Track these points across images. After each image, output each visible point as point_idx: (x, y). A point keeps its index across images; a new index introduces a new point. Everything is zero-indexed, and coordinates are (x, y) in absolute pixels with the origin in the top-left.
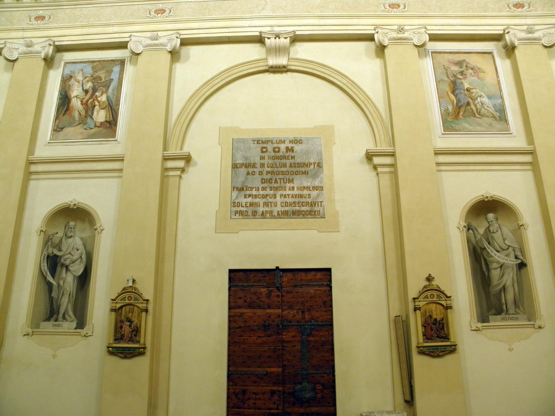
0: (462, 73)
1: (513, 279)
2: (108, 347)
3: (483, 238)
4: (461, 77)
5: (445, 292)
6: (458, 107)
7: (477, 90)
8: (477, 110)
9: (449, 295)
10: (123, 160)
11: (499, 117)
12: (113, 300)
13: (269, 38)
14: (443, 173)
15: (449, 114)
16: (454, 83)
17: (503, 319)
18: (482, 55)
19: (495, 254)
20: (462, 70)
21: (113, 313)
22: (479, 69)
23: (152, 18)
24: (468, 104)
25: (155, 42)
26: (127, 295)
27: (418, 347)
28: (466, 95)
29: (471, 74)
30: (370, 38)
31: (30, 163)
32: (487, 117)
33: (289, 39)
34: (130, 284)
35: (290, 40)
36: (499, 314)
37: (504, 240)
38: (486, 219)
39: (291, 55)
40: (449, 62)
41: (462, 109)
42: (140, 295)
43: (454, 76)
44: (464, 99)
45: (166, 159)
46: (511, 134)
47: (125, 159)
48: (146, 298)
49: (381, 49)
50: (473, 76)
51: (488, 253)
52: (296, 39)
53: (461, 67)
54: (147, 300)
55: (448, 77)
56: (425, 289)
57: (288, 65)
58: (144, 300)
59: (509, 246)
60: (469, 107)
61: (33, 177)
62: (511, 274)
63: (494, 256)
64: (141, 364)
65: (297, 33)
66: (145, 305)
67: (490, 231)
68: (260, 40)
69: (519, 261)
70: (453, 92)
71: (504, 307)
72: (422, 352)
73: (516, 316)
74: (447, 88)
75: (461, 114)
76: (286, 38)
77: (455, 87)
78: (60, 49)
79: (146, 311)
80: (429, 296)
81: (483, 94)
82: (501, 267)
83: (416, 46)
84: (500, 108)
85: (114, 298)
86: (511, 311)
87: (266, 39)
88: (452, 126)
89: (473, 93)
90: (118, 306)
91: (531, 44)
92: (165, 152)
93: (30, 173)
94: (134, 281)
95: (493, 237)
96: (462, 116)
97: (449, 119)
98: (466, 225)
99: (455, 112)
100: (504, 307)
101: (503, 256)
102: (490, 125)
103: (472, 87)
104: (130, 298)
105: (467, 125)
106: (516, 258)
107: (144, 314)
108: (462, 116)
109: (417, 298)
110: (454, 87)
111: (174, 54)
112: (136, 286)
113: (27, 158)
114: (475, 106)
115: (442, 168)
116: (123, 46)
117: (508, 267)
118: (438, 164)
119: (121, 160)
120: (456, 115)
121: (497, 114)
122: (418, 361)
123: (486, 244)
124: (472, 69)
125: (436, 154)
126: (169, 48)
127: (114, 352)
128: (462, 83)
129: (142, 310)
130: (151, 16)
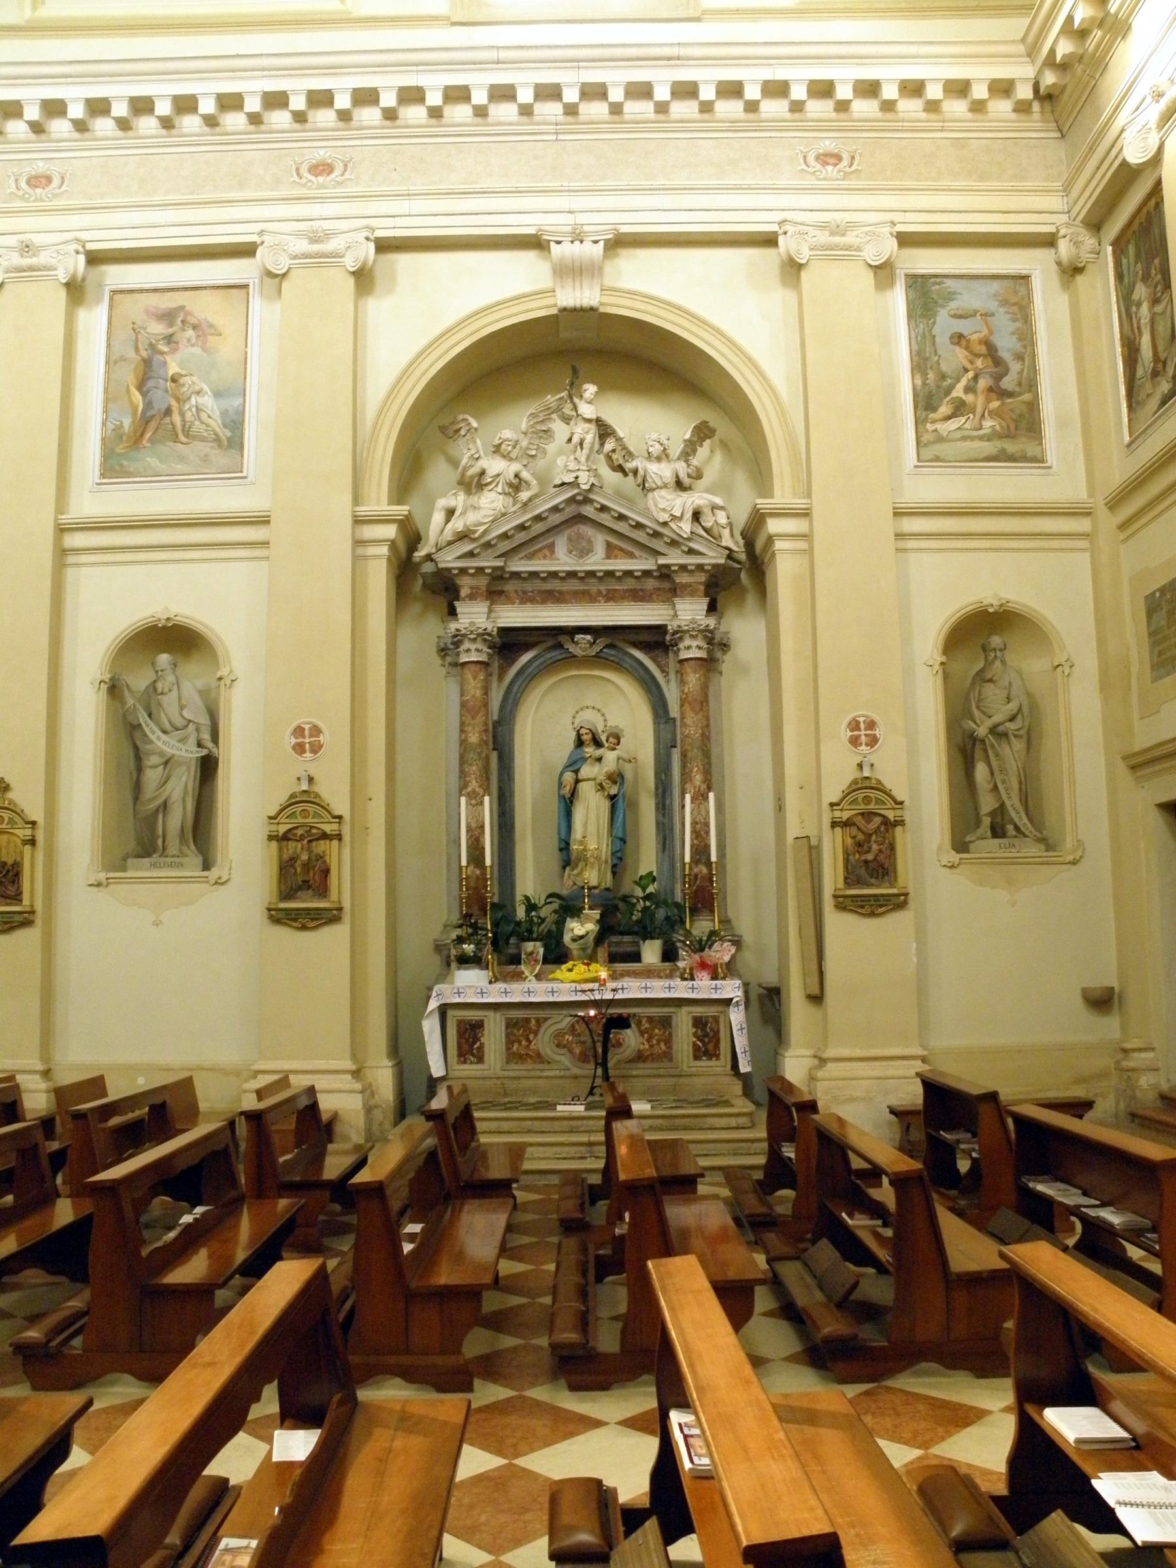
0: (169, 339)
1: (186, 787)
2: (269, 910)
3: (138, 706)
4: (166, 349)
5: (893, 793)
6: (144, 421)
7: (195, 379)
8: (184, 426)
9: (899, 799)
10: (268, 522)
11: (229, 439)
12: (270, 818)
13: (559, 243)
14: (912, 556)
15: (121, 438)
16: (147, 363)
17: (154, 866)
18: (222, 291)
19: (158, 738)
20: (170, 331)
21: (274, 844)
22: (211, 326)
23: (304, 185)
24: (168, 412)
25: (837, 239)
26: (298, 808)
27: (835, 897)
28: (167, 391)
29: (189, 340)
30: (769, 241)
31: (61, 530)
32: (204, 439)
33: (602, 243)
34: (305, 787)
35: (605, 245)
36: (149, 855)
37: (182, 708)
38: (153, 664)
40: (147, 312)
41: (153, 425)
42: (20, 814)
43: (152, 347)
44: (161, 400)
45: (358, 521)
46: (1050, 468)
47: (272, 519)
48: (337, 813)
49: (793, 269)
50: (193, 345)
51: (146, 735)
52: (619, 243)
53: (171, 325)
54: (340, 817)
55: (137, 349)
56: (854, 787)
59: (190, 721)
60: (167, 420)
61: (71, 559)
62: (184, 779)
63: (155, 741)
64: (895, 923)
65: (624, 229)
66: (335, 827)
67: (155, 690)
68: (535, 243)
69: (205, 752)
70: (140, 387)
71: (160, 842)
72: (843, 904)
73: (180, 860)
74: (127, 375)
75: (148, 435)
76: (596, 242)
77: (147, 372)
78: (95, 259)
80: (860, 799)
81: (206, 388)
82: (166, 763)
83: (871, 266)
84: (234, 418)
85: (273, 814)
86: (173, 849)
87: (552, 244)
88: (121, 466)
89: (184, 385)
90: (282, 829)
91: (320, 265)
92: (357, 509)
93: (64, 550)
94: (311, 780)
95: (159, 704)
96: (149, 440)
97: (119, 450)
98: (107, 677)
99: (135, 432)
100: (160, 842)
101: (173, 742)
102: (205, 459)
103: (183, 372)
104: (867, 800)
105: (153, 462)
106: (200, 745)
108: (149, 440)
109: (838, 804)
110: (145, 374)
111: (363, 278)
112: (316, 789)
113: (56, 519)
114: (182, 415)
115: (912, 544)
116: (246, 251)
117: (180, 764)
118: (899, 536)
119: (264, 521)
120: (136, 440)
121: (224, 434)
122: (837, 924)
123: (143, 717)
124: (195, 327)
126: (351, 263)
127: (278, 917)
128: (166, 363)
130: (303, 181)
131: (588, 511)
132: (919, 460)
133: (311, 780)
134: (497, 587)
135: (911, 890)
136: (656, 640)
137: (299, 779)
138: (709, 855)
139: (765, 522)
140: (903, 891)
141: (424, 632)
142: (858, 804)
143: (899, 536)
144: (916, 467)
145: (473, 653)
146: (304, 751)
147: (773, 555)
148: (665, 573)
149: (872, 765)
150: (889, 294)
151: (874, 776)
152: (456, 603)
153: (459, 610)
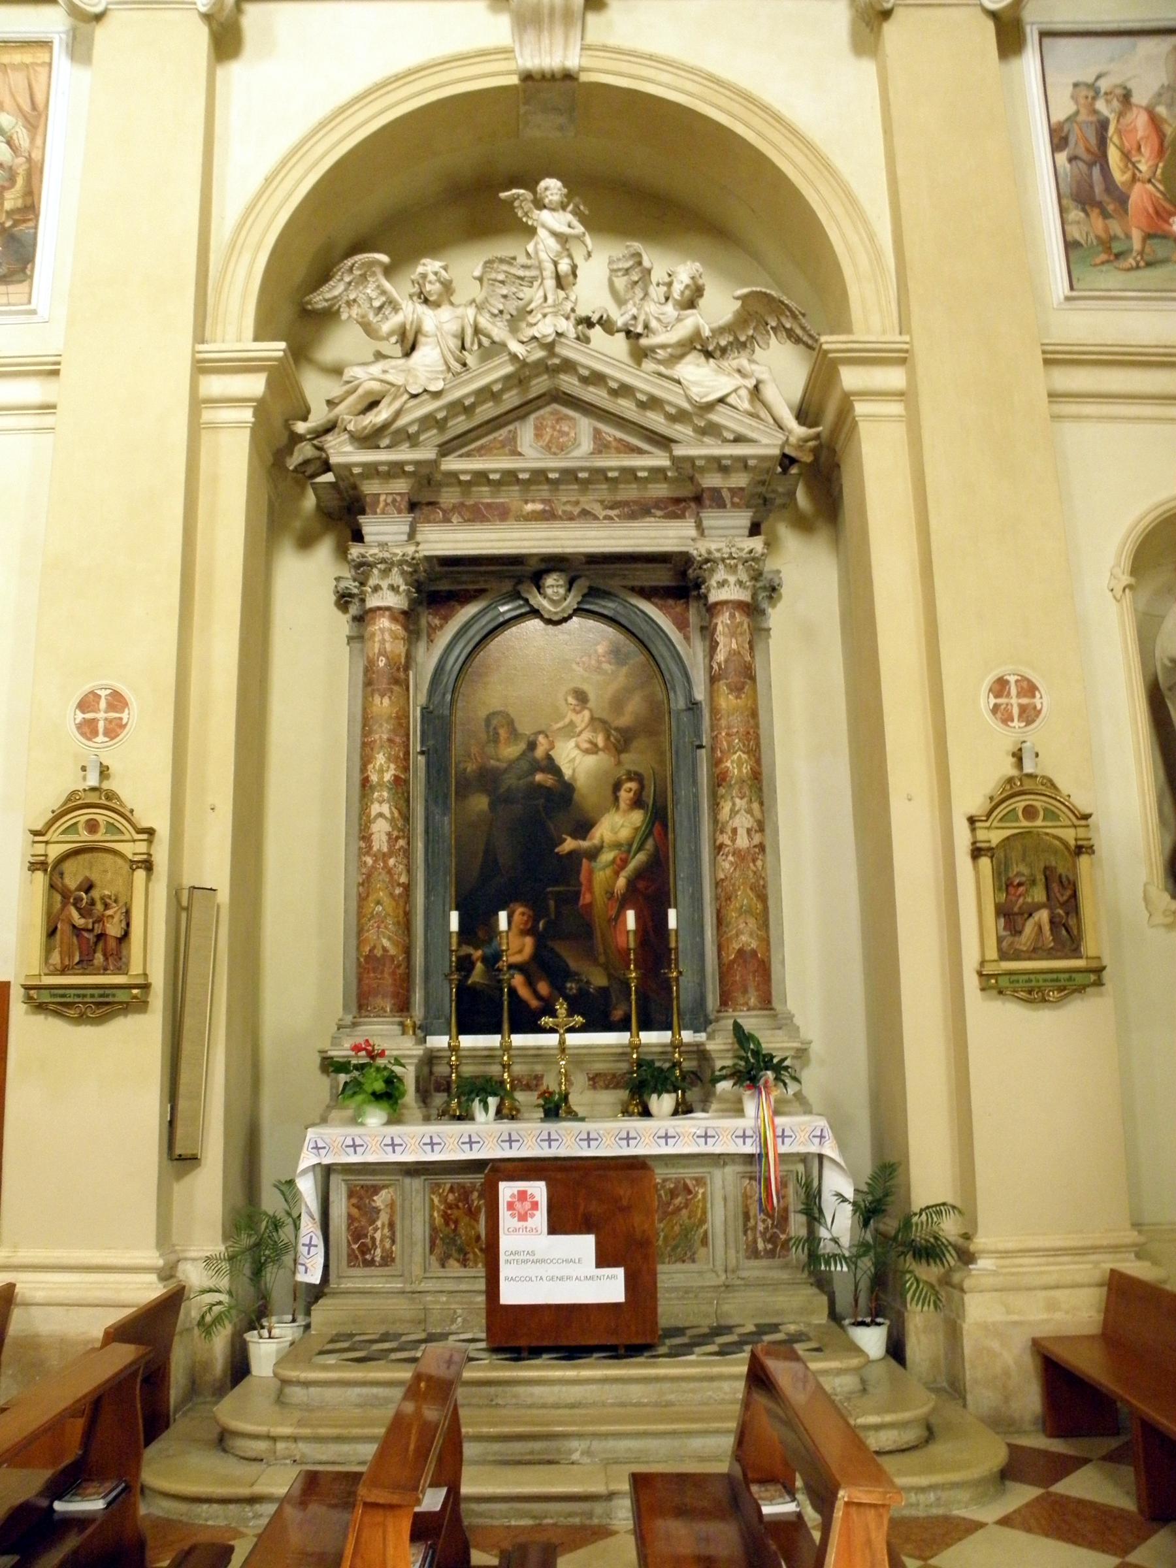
10: (56, 373)
12: (36, 833)
21: (39, 875)
34: (93, 780)
39: (590, 38)
45: (202, 368)
48: (145, 824)
54: (150, 832)
57: (582, 69)
58: (140, 831)
64: (139, 1038)
66: (142, 847)
72: (992, 984)
79: (148, 865)
90: (54, 851)
94: (104, 772)
104: (1030, 812)
107: (140, 874)
115: (1071, 409)
118: (1053, 396)
125: (1051, 361)
129: (134, 865)
131: (569, 383)
132: (1072, 288)
133: (104, 772)
134: (424, 498)
135: (1106, 961)
136: (680, 581)
137: (84, 769)
138: (905, 1475)
139: (838, 371)
140: (1094, 964)
141: (308, 579)
142: (1017, 820)
143: (1052, 395)
144: (1067, 299)
145: (389, 595)
146: (95, 733)
147: (855, 424)
148: (687, 469)
149: (1037, 755)
150: (1015, 64)
151: (1039, 772)
152: (362, 519)
153: (366, 530)
